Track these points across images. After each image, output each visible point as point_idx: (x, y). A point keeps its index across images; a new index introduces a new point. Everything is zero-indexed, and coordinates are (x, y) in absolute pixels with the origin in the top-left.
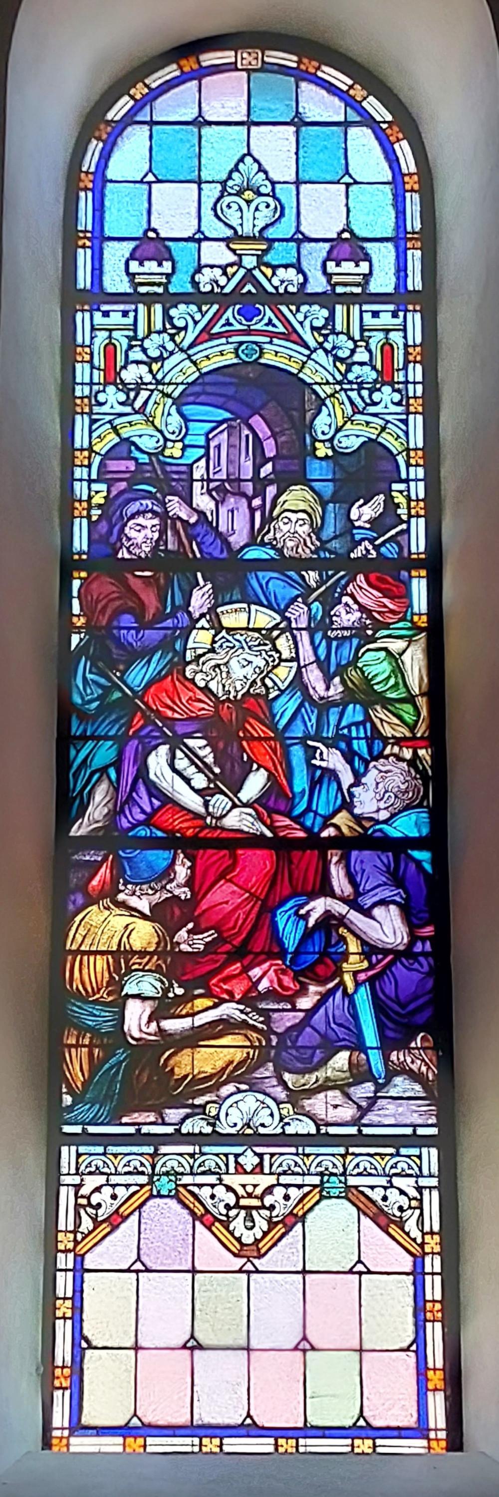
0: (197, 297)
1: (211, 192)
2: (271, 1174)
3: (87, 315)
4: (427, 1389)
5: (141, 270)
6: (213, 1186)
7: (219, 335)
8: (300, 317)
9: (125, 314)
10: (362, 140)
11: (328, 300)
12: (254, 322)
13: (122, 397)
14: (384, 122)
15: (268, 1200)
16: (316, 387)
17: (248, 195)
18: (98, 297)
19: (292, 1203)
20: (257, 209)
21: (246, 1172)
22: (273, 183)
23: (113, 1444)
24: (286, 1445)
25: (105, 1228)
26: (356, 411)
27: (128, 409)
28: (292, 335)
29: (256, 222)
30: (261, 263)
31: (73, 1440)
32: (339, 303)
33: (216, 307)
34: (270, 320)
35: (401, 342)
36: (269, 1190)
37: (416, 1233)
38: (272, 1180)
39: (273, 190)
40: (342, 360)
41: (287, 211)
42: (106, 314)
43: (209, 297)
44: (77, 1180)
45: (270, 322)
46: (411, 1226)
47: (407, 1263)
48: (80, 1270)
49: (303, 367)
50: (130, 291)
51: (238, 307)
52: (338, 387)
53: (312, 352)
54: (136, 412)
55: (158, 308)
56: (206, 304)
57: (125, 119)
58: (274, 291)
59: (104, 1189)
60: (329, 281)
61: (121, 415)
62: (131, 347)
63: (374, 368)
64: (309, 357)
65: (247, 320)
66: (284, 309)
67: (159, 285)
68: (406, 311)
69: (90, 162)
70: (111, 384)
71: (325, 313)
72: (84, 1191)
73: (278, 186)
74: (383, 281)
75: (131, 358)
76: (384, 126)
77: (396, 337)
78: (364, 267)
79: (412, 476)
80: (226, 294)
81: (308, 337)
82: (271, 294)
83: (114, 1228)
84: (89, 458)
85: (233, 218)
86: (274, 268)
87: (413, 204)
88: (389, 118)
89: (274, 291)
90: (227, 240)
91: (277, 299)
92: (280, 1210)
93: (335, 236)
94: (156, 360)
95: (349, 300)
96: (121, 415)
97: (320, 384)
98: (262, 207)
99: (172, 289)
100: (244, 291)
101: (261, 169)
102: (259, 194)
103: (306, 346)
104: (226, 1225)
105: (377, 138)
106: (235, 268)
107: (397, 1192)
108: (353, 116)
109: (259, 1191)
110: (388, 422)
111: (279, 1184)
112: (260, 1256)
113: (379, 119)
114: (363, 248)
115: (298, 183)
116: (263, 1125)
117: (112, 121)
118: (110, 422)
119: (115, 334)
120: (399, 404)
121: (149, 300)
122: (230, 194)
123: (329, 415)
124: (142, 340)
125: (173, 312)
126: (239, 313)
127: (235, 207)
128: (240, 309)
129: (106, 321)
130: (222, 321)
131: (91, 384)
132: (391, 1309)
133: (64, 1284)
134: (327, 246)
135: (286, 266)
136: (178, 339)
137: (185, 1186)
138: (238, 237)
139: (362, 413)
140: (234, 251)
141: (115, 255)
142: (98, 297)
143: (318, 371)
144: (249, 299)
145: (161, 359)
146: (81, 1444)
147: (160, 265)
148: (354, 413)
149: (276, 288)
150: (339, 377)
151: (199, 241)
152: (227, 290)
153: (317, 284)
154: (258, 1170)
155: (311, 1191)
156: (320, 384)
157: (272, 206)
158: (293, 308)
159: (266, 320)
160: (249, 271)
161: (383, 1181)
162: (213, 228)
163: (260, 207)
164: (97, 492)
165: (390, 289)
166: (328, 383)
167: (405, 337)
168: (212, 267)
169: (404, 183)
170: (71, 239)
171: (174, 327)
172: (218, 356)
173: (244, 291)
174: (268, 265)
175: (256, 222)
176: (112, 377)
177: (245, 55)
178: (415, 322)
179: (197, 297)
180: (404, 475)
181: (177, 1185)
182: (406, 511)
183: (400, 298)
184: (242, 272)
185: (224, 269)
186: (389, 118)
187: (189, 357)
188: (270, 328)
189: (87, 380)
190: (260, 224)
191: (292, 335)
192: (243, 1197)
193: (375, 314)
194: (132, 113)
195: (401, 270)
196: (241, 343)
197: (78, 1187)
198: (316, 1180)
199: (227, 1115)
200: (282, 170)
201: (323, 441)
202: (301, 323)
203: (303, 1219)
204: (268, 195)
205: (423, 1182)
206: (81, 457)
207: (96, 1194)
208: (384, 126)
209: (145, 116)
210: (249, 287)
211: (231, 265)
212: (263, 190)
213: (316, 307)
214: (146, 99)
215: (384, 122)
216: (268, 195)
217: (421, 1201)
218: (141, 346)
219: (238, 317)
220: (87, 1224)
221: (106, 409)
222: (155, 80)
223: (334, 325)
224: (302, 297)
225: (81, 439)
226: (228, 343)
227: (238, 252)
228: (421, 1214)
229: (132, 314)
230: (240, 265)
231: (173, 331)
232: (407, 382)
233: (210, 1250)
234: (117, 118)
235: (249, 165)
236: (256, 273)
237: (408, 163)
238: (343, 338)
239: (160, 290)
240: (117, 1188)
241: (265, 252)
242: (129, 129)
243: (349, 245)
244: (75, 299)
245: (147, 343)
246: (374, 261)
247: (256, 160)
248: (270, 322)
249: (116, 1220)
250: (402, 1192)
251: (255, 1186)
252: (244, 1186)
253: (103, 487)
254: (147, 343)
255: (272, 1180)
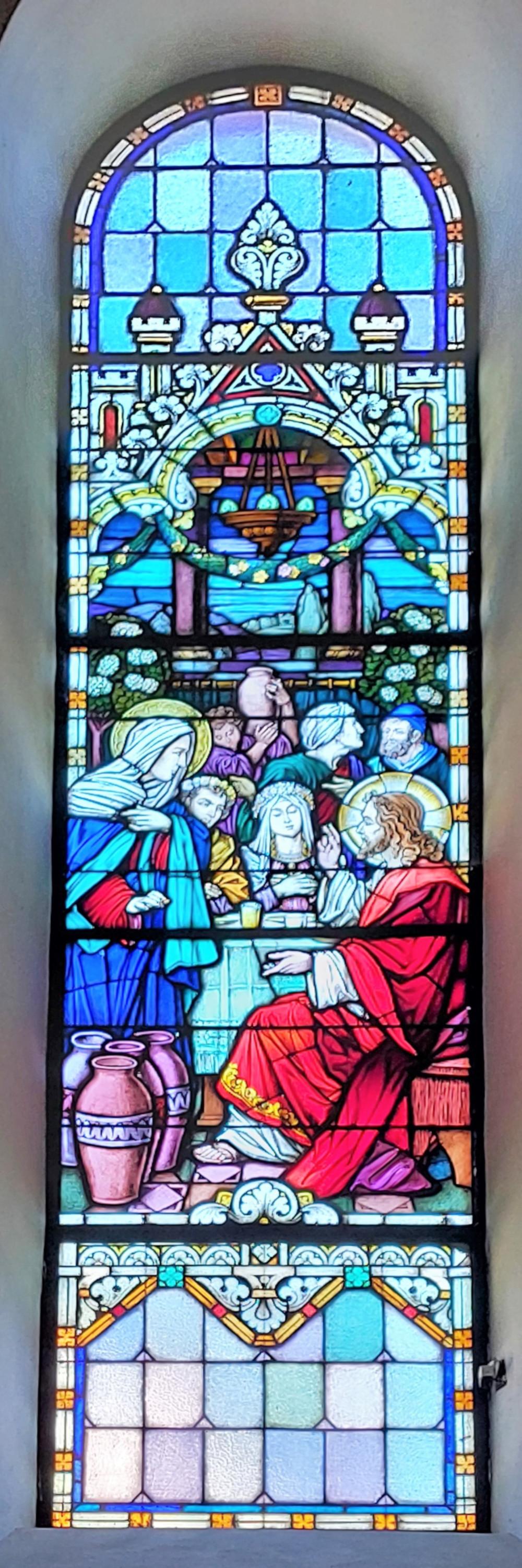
0: (207, 357)
1: (224, 243)
2: (288, 1265)
3: (85, 375)
4: (456, 1475)
5: (145, 328)
6: (223, 1278)
7: (235, 396)
8: (330, 375)
9: (124, 374)
10: (398, 182)
11: (360, 358)
12: (275, 380)
13: (123, 463)
14: (426, 163)
15: (284, 1292)
16: (344, 450)
17: (268, 246)
18: (97, 359)
19: (121, 1295)
20: (277, 261)
21: (262, 1264)
22: (297, 233)
23: (118, 1520)
24: (302, 1522)
25: (107, 1319)
26: (390, 475)
27: (126, 476)
28: (315, 394)
29: (276, 275)
30: (279, 321)
31: (76, 1516)
32: (371, 362)
33: (226, 369)
34: (293, 378)
35: (442, 403)
36: (284, 1281)
37: (446, 1325)
38: (289, 1272)
39: (297, 239)
40: (375, 422)
41: (311, 257)
42: (102, 374)
43: (225, 357)
44: (77, 1271)
45: (243, 382)
46: (441, 1318)
47: (434, 1352)
48: (82, 1361)
49: (330, 426)
50: (133, 349)
51: (254, 366)
52: (369, 450)
53: (340, 413)
54: (138, 480)
55: (165, 371)
56: (216, 364)
57: (126, 164)
58: (296, 349)
59: (105, 1281)
60: (134, 340)
61: (124, 483)
62: (135, 410)
63: (411, 429)
64: (336, 419)
65: (264, 379)
66: (308, 367)
67: (165, 344)
68: (446, 369)
69: (85, 211)
70: (111, 450)
71: (356, 371)
72: (86, 1282)
73: (303, 237)
74: (421, 338)
75: (134, 423)
76: (427, 168)
77: (435, 397)
78: (399, 322)
79: (453, 546)
80: (241, 353)
81: (335, 396)
82: (293, 352)
83: (118, 1318)
84: (87, 529)
85: (250, 270)
86: (297, 324)
87: (456, 256)
88: (432, 159)
89: (296, 349)
90: (242, 296)
91: (301, 358)
92: (110, 1300)
93: (364, 289)
94: (162, 424)
95: (381, 358)
96: (124, 483)
97: (349, 447)
98: (283, 258)
99: (179, 349)
100: (263, 350)
101: (282, 217)
102: (280, 245)
103: (336, 409)
104: (238, 1315)
105: (417, 180)
106: (251, 324)
107: (424, 1282)
108: (388, 156)
109: (273, 1283)
110: (426, 487)
111: (295, 1276)
112: (278, 1345)
113: (419, 159)
114: (399, 302)
115: (324, 230)
116: (279, 1213)
117: (110, 167)
118: (111, 491)
119: (118, 398)
120: (438, 467)
121: (156, 360)
122: (245, 245)
123: (360, 480)
124: (148, 403)
125: (179, 374)
126: (256, 372)
127: (252, 257)
128: (256, 368)
129: (412, 379)
130: (238, 380)
131: (89, 450)
132: (419, 1395)
133: (64, 1377)
134: (357, 299)
135: (310, 323)
136: (187, 400)
137: (193, 1277)
138: (254, 291)
139: (397, 477)
140: (248, 307)
141: (114, 313)
142: (97, 359)
143: (348, 432)
144: (266, 356)
145: (169, 421)
146: (83, 1520)
147: (167, 322)
148: (388, 478)
149: (298, 346)
150: (372, 441)
151: (211, 297)
152: (243, 348)
153: (346, 342)
154: (275, 1260)
155: (330, 1282)
156: (349, 447)
157: (295, 258)
158: (321, 368)
159: (288, 379)
160: (267, 327)
161: (413, 1272)
162: (225, 281)
163: (280, 259)
164: (97, 566)
165: (430, 347)
166: (357, 446)
167: (446, 396)
168: (225, 323)
169: (447, 232)
170: (65, 289)
171: (182, 389)
172: (234, 418)
173: (263, 350)
174: (287, 322)
175: (276, 275)
176: (112, 443)
177: (262, 92)
178: (457, 377)
179: (207, 357)
180: (443, 546)
181: (185, 1276)
182: (447, 584)
183: (439, 356)
184: (258, 331)
185: (239, 324)
186: (432, 159)
187: (201, 421)
188: (293, 388)
189: (84, 446)
190: (280, 276)
191: (315, 394)
192: (258, 1289)
193: (412, 371)
194: (132, 158)
195: (441, 325)
196: (258, 405)
197: (79, 1278)
198: (338, 1271)
199: (241, 1202)
200: (306, 215)
201: (353, 510)
202: (329, 382)
203: (321, 1311)
204: (289, 245)
205: (454, 1272)
206: (77, 528)
207: (97, 1286)
208: (427, 168)
209: (147, 160)
210: (267, 347)
211: (247, 321)
212: (283, 240)
213: (347, 365)
214: (145, 145)
215: (426, 163)
216: (289, 245)
217: (451, 1291)
218: (145, 409)
219: (255, 376)
220: (88, 1315)
221: (105, 476)
222: (155, 123)
223: (364, 384)
224: (328, 357)
225: (77, 506)
226: (246, 404)
227: (255, 308)
228: (451, 1307)
229: (132, 376)
230: (256, 322)
231: (182, 394)
232: (448, 445)
233: (223, 1345)
234: (116, 164)
235: (267, 214)
236: (275, 329)
237: (451, 208)
238: (375, 397)
239: (167, 349)
240: (308, 1280)
241: (285, 308)
242: (132, 174)
243: (381, 300)
244: (67, 358)
245: (153, 407)
246: (410, 316)
247: (276, 207)
248: (292, 382)
249: (120, 1312)
250: (429, 1281)
251: (270, 1277)
252: (258, 1277)
253: (103, 560)
254: (153, 407)
255: (289, 1272)
